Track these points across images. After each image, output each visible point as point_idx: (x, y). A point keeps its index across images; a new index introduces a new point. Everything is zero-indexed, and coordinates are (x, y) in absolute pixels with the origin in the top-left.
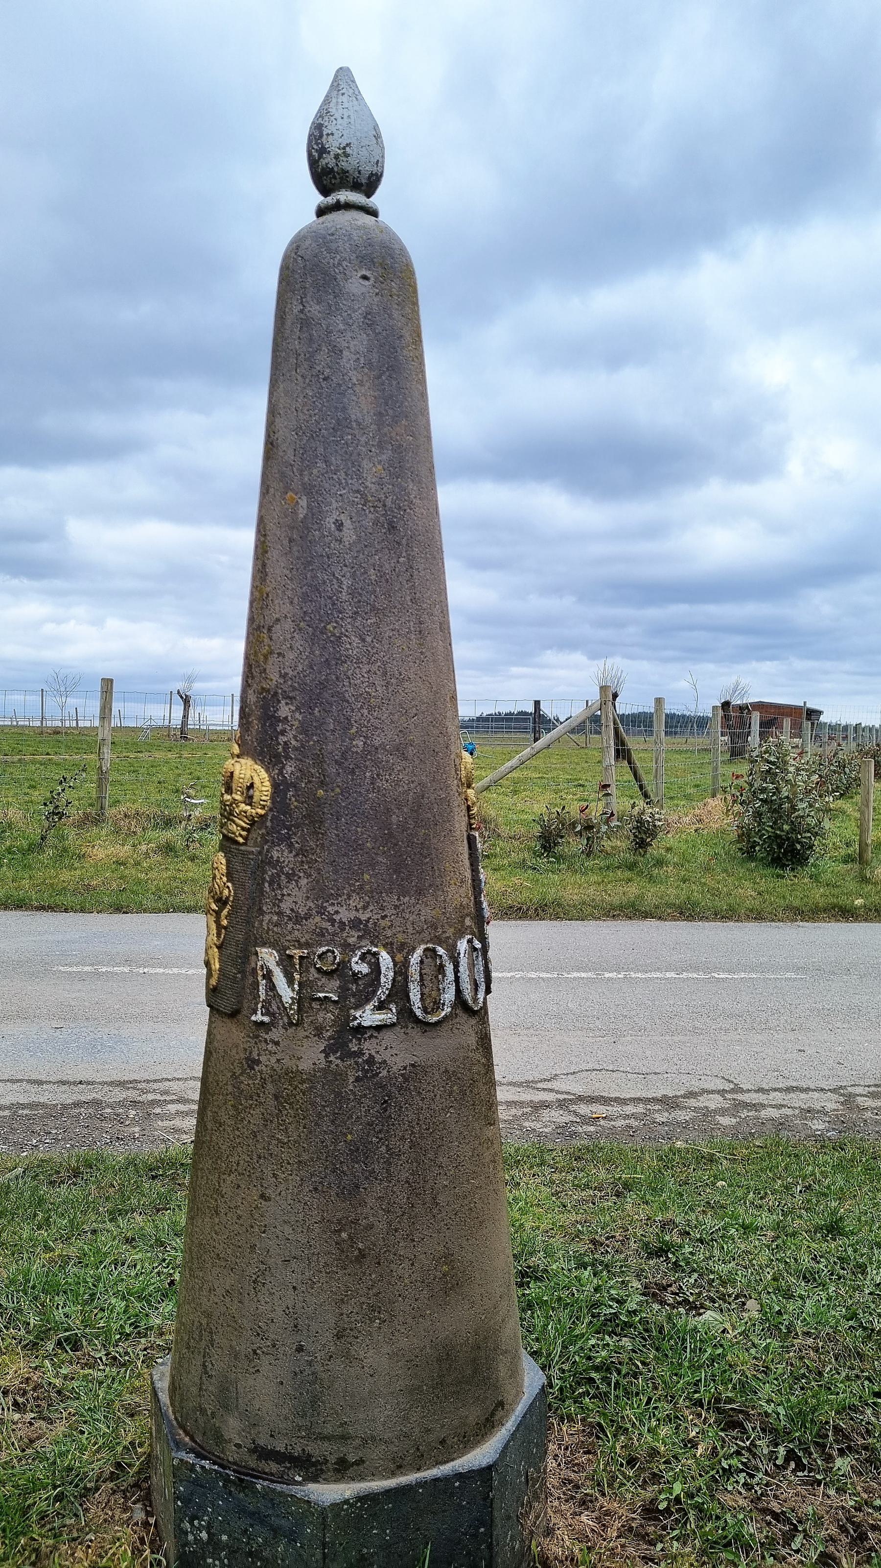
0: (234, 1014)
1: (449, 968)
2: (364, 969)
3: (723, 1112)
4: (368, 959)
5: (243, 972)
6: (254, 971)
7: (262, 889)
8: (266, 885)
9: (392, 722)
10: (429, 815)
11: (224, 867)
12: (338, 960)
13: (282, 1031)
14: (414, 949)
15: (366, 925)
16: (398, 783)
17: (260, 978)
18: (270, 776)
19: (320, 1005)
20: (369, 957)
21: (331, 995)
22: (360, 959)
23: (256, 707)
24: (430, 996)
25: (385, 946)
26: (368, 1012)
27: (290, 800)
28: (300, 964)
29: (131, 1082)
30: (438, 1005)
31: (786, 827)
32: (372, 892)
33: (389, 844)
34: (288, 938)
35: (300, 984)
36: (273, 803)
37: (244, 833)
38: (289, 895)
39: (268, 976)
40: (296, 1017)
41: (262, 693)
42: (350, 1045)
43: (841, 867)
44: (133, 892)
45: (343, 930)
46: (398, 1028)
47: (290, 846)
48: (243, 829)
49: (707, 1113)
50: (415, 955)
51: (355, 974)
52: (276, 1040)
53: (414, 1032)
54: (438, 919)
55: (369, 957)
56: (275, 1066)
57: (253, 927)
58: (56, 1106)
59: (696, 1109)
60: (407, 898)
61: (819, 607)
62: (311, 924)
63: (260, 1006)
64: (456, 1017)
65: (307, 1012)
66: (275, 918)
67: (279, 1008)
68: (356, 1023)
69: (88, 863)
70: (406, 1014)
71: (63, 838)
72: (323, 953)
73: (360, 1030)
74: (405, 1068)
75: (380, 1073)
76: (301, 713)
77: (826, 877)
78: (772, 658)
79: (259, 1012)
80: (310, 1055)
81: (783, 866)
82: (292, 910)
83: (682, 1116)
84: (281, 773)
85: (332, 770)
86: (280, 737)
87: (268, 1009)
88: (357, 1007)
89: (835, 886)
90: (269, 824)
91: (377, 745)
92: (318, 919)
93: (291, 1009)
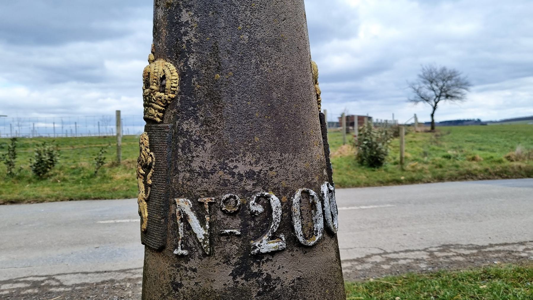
0: (161, 250)
1: (319, 205)
2: (260, 209)
3: (383, 263)
4: (262, 201)
5: (165, 217)
6: (174, 216)
7: (177, 154)
8: (180, 150)
9: (269, 22)
10: (298, 94)
11: (148, 142)
12: (239, 203)
13: (198, 261)
14: (293, 193)
15: (258, 176)
16: (275, 68)
17: (178, 221)
18: (177, 68)
19: (227, 239)
20: (262, 200)
21: (235, 231)
22: (256, 201)
23: (164, 20)
24: (307, 226)
25: (273, 191)
26: (265, 242)
27: (194, 84)
28: (210, 208)
29: (128, 270)
30: (313, 232)
31: (375, 153)
32: (261, 150)
33: (272, 114)
34: (199, 189)
35: (210, 224)
36: (181, 88)
37: (161, 114)
38: (197, 156)
39: (185, 219)
40: (209, 250)
41: (168, 8)
42: (252, 268)
43: (393, 166)
44: (132, 191)
45: (241, 180)
46: (287, 252)
47: (196, 119)
48: (160, 111)
49: (377, 264)
50: (296, 197)
51: (253, 213)
52: (194, 267)
53: (298, 253)
54: (308, 170)
55: (262, 200)
56: (194, 288)
57: (172, 183)
58: (93, 284)
59: (372, 263)
60: (287, 154)
61: (370, 83)
62: (215, 177)
63: (179, 242)
64: (324, 240)
65: (217, 245)
66: (188, 175)
67: (194, 243)
68: (256, 251)
69: (114, 181)
70: (292, 241)
71: (104, 172)
72: (227, 199)
73: (260, 255)
74: (293, 282)
75: (275, 287)
76: (198, 17)
77: (390, 170)
78: (355, 100)
79: (179, 247)
80: (222, 278)
81: (374, 167)
82: (200, 167)
83: (368, 266)
84: (186, 64)
85: (225, 59)
86: (184, 37)
87: (186, 245)
88: (255, 238)
89: (393, 173)
90: (179, 104)
91: (259, 38)
92: (221, 173)
93: (204, 244)
